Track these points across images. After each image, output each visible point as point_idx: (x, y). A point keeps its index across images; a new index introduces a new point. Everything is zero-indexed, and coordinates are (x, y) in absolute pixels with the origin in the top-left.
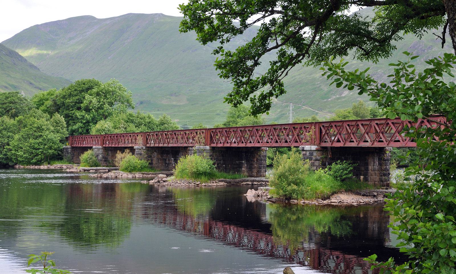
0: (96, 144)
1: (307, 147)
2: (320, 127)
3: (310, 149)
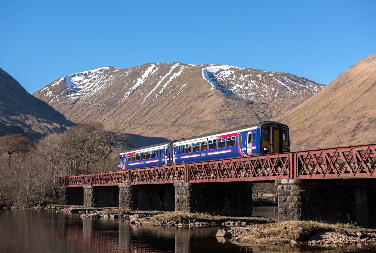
3: (287, 183)
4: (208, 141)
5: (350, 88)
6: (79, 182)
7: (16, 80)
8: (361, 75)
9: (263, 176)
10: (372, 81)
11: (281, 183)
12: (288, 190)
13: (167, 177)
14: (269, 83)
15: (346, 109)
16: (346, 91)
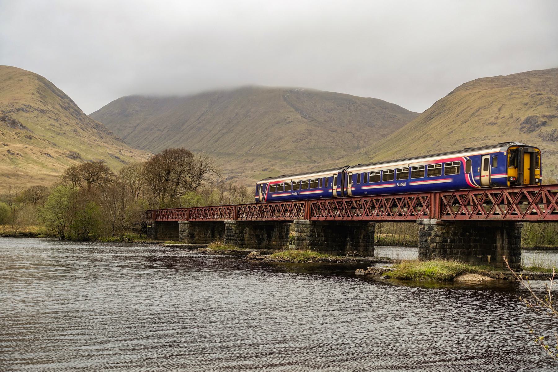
0: (181, 219)
1: (426, 221)
2: (441, 199)
4: (410, 168)
5: (447, 117)
6: (171, 216)
7: (71, 99)
8: (459, 103)
9: (399, 215)
10: (471, 110)
11: (423, 223)
12: (429, 230)
13: (270, 214)
14: (356, 110)
15: (442, 141)
16: (443, 120)
